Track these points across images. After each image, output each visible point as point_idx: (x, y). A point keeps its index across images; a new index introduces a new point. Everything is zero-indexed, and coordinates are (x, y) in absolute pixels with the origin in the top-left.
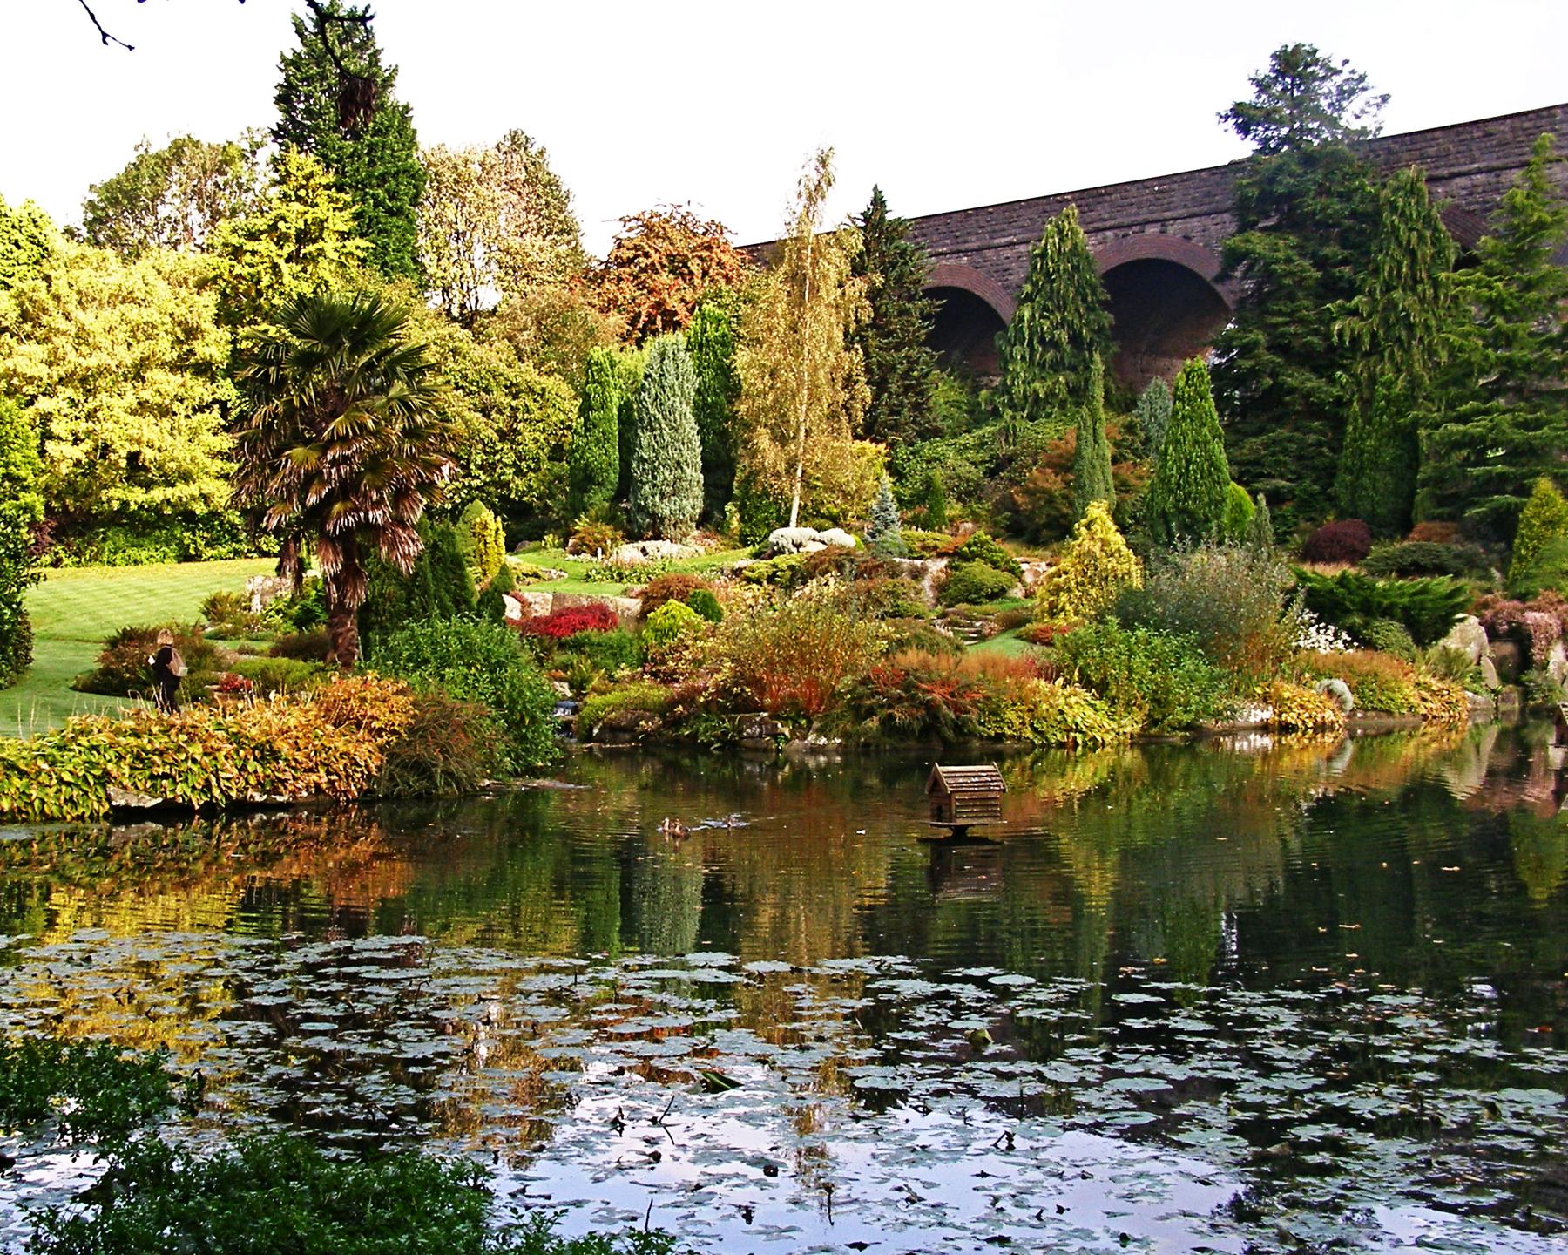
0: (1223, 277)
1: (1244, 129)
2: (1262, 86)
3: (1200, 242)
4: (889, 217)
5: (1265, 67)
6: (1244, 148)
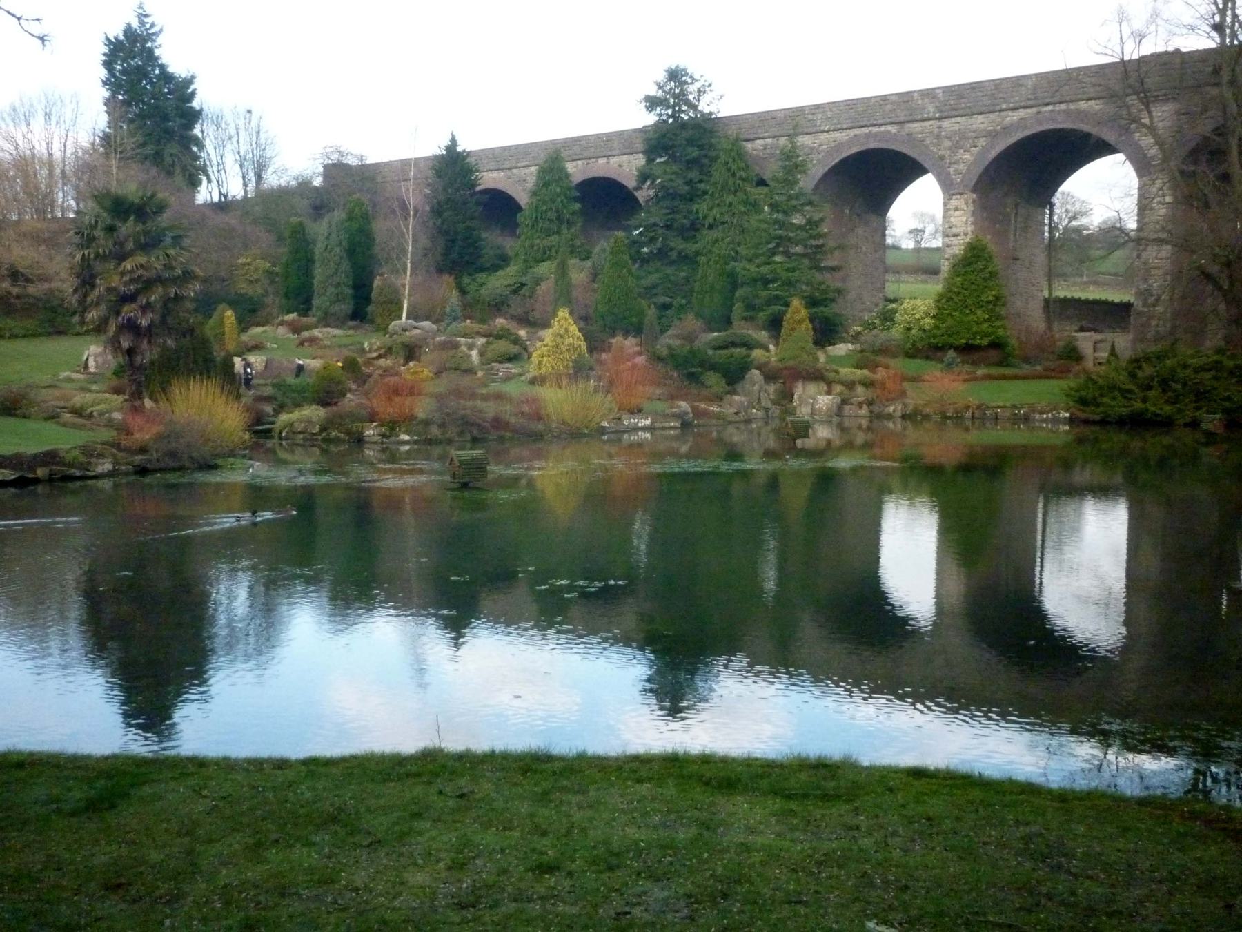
3: (626, 168)
6: (650, 119)
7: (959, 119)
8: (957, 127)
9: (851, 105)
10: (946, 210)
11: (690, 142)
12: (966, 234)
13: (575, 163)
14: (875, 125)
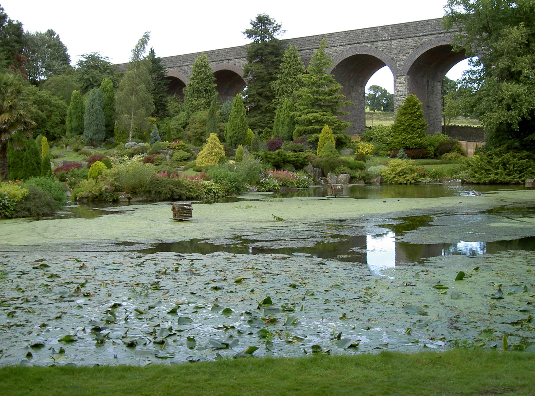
0: (246, 76)
1: (249, 37)
2: (254, 25)
3: (239, 66)
4: (156, 57)
5: (254, 20)
6: (251, 41)
7: (399, 40)
8: (399, 44)
9: (348, 33)
10: (395, 83)
11: (271, 53)
12: (405, 95)
13: (212, 63)
14: (359, 43)
